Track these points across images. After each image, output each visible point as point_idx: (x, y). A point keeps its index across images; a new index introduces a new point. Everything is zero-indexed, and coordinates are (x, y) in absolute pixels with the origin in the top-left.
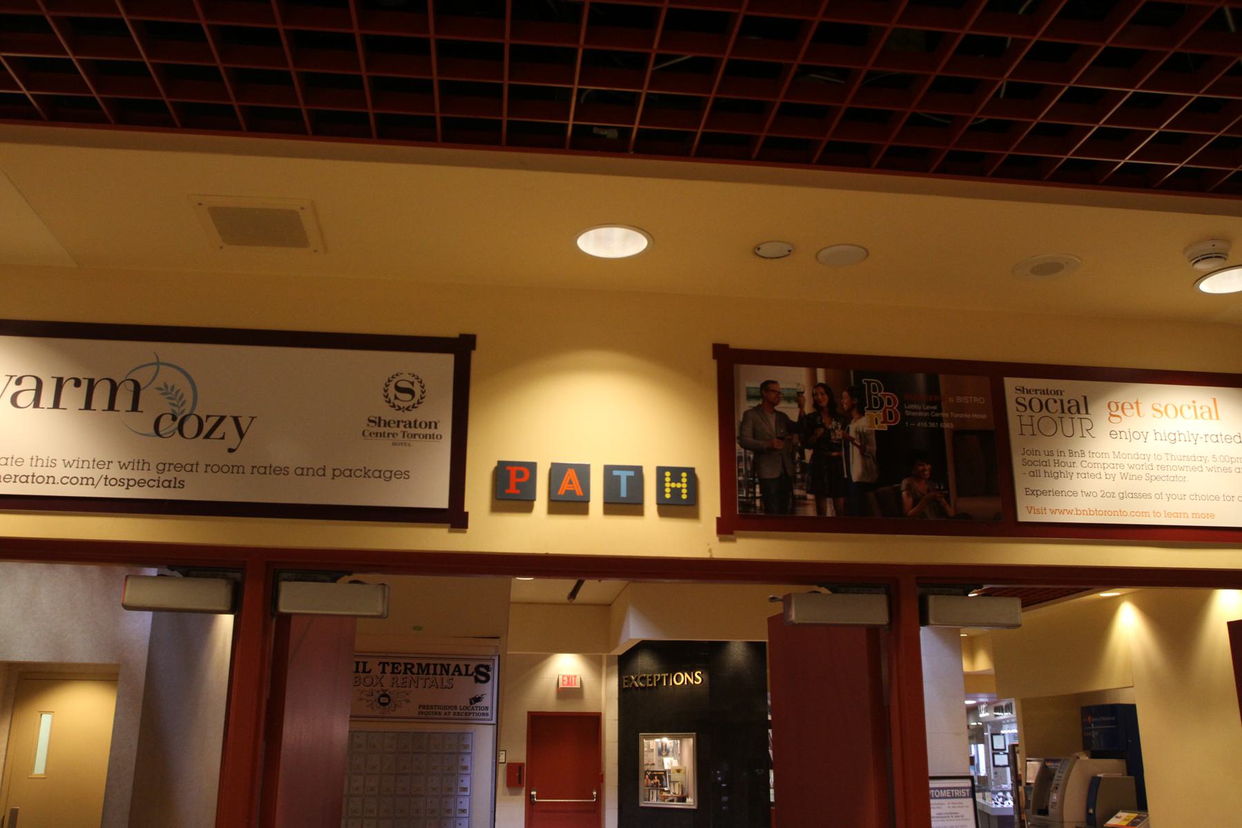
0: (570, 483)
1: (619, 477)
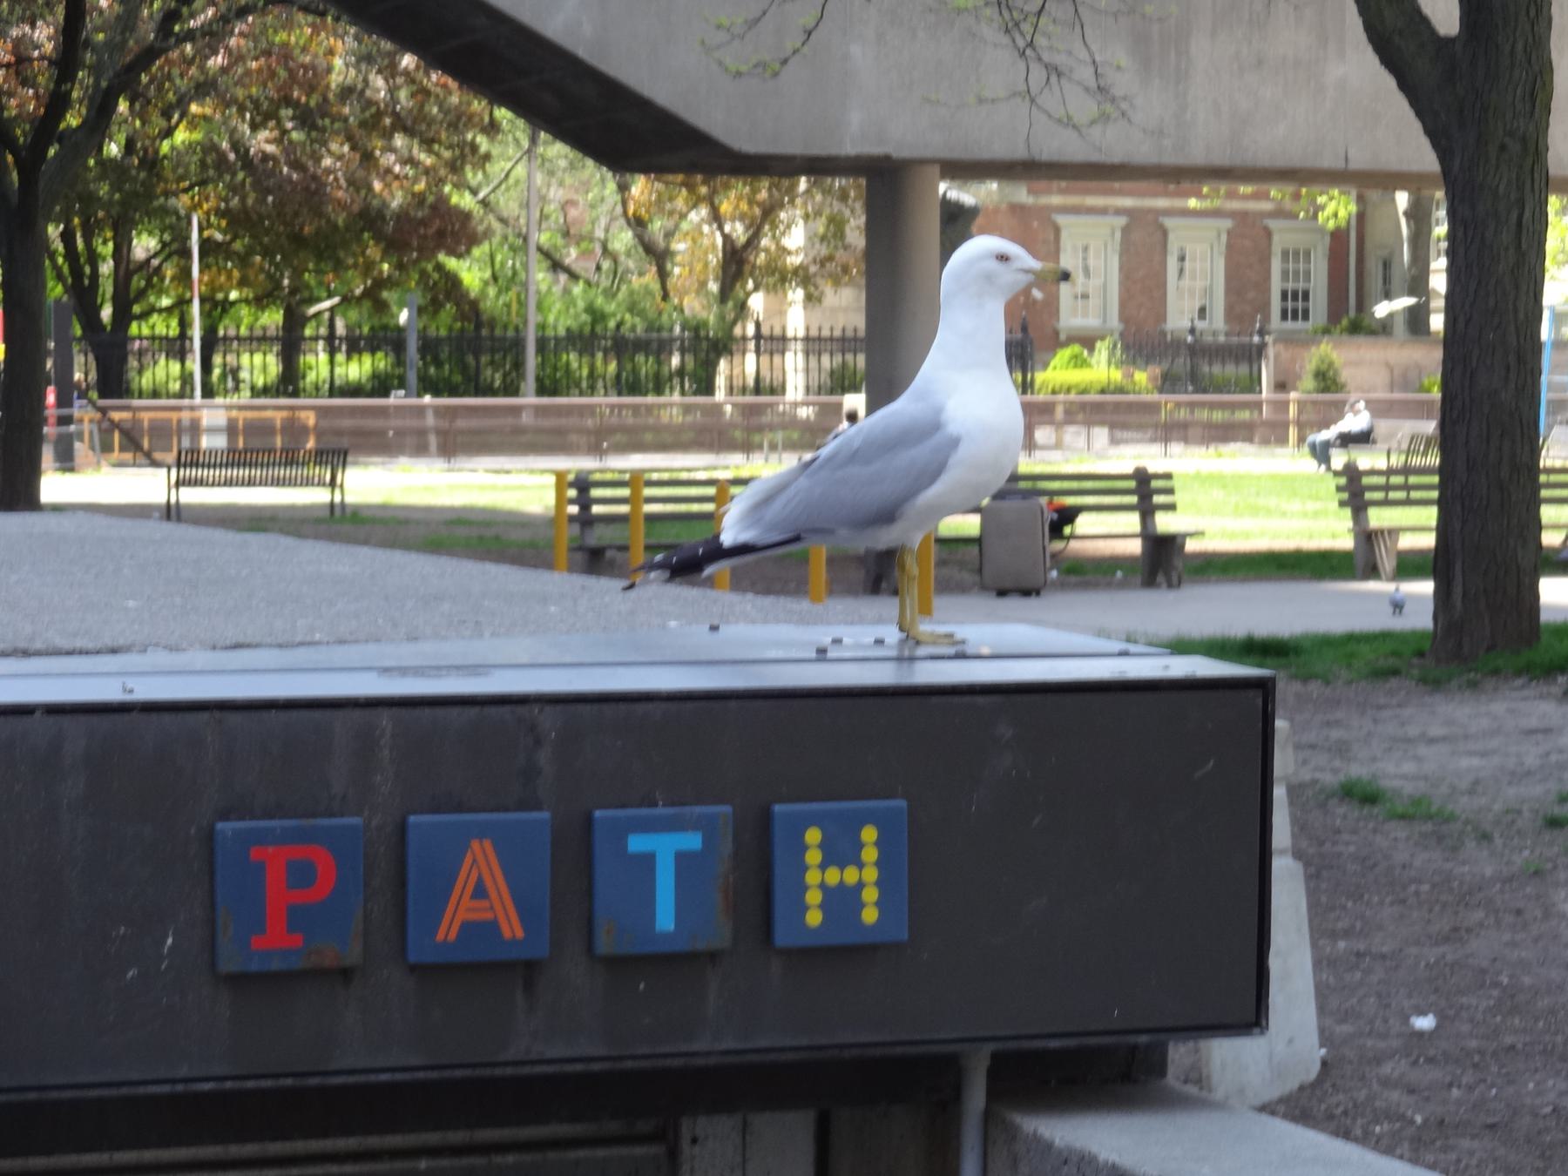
0: (480, 892)
1: (648, 860)
